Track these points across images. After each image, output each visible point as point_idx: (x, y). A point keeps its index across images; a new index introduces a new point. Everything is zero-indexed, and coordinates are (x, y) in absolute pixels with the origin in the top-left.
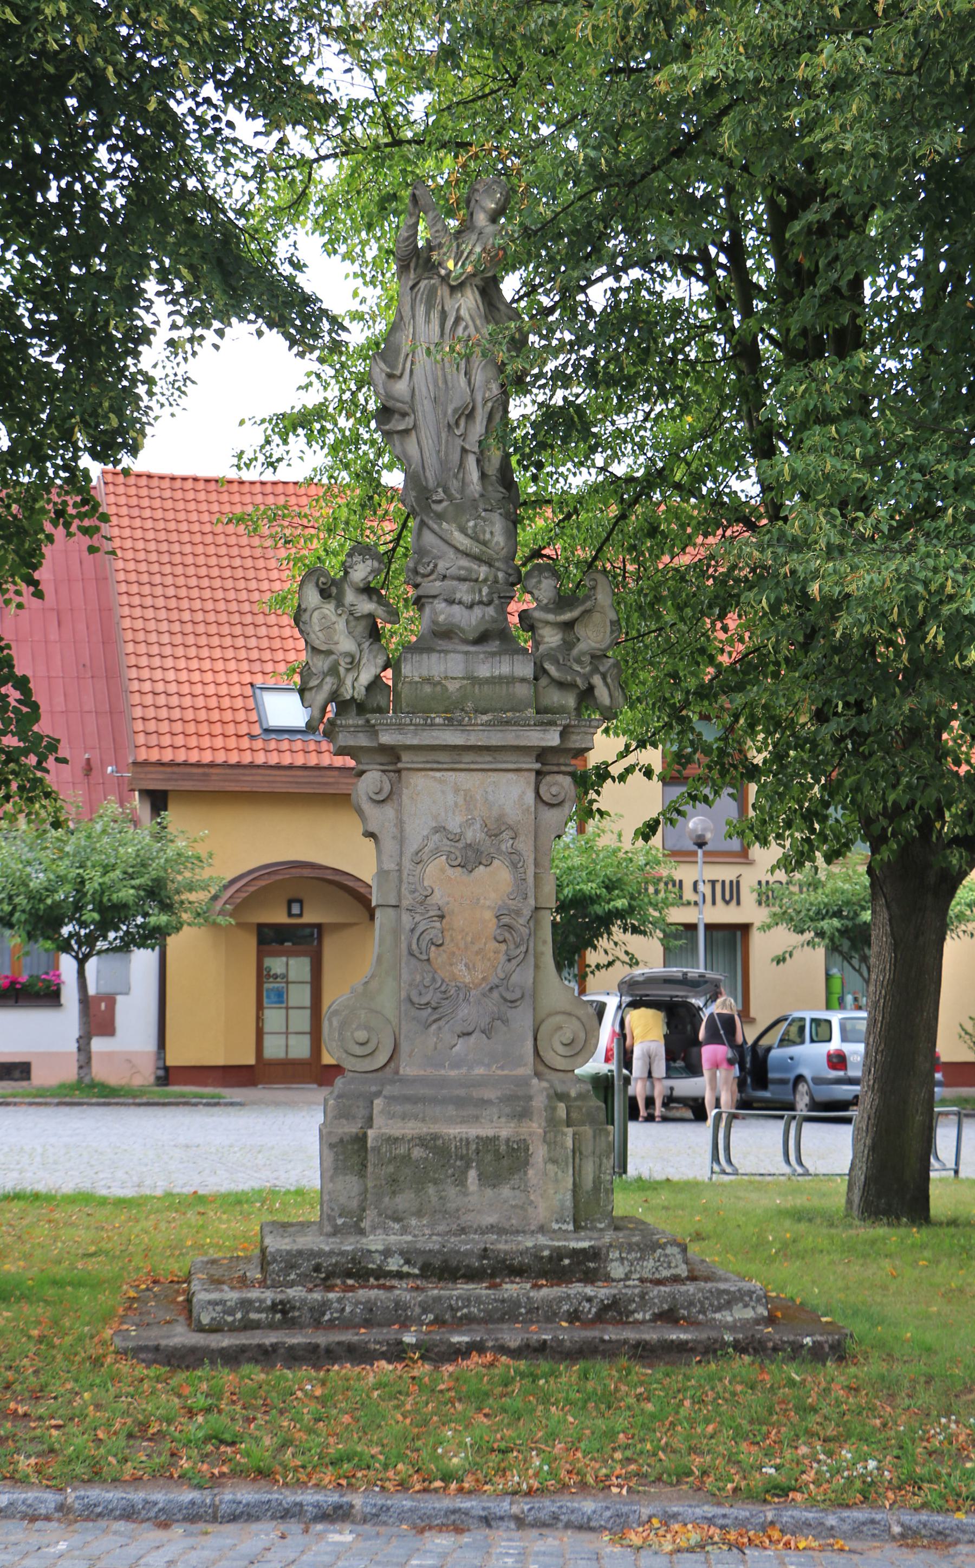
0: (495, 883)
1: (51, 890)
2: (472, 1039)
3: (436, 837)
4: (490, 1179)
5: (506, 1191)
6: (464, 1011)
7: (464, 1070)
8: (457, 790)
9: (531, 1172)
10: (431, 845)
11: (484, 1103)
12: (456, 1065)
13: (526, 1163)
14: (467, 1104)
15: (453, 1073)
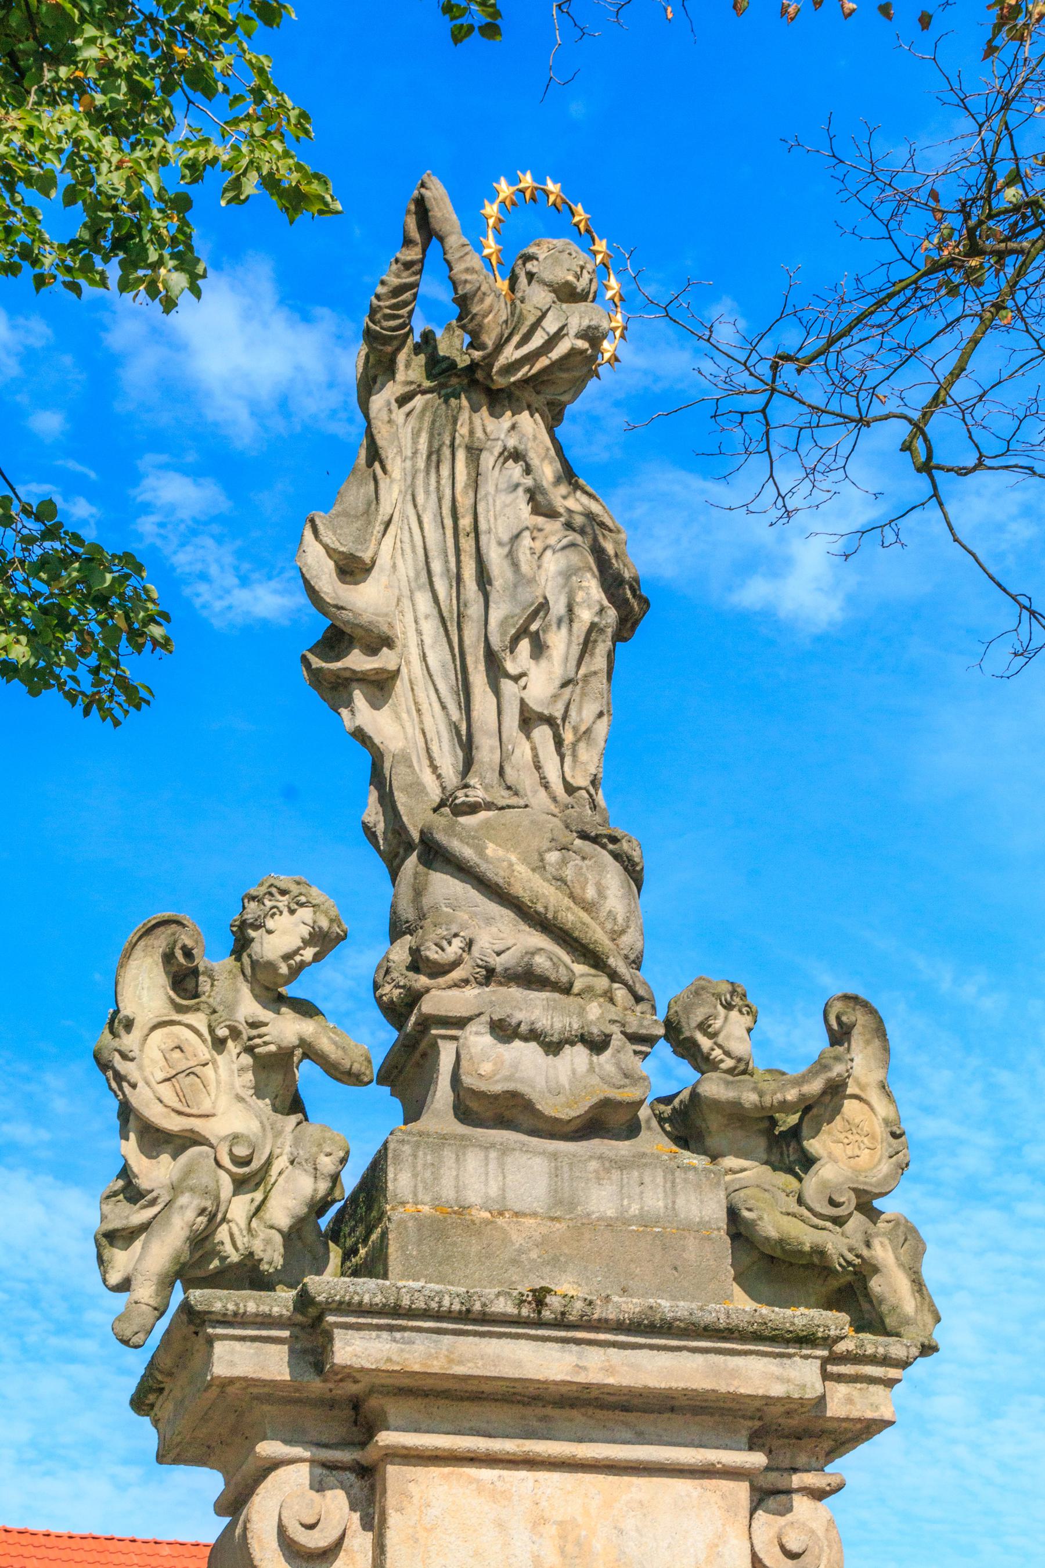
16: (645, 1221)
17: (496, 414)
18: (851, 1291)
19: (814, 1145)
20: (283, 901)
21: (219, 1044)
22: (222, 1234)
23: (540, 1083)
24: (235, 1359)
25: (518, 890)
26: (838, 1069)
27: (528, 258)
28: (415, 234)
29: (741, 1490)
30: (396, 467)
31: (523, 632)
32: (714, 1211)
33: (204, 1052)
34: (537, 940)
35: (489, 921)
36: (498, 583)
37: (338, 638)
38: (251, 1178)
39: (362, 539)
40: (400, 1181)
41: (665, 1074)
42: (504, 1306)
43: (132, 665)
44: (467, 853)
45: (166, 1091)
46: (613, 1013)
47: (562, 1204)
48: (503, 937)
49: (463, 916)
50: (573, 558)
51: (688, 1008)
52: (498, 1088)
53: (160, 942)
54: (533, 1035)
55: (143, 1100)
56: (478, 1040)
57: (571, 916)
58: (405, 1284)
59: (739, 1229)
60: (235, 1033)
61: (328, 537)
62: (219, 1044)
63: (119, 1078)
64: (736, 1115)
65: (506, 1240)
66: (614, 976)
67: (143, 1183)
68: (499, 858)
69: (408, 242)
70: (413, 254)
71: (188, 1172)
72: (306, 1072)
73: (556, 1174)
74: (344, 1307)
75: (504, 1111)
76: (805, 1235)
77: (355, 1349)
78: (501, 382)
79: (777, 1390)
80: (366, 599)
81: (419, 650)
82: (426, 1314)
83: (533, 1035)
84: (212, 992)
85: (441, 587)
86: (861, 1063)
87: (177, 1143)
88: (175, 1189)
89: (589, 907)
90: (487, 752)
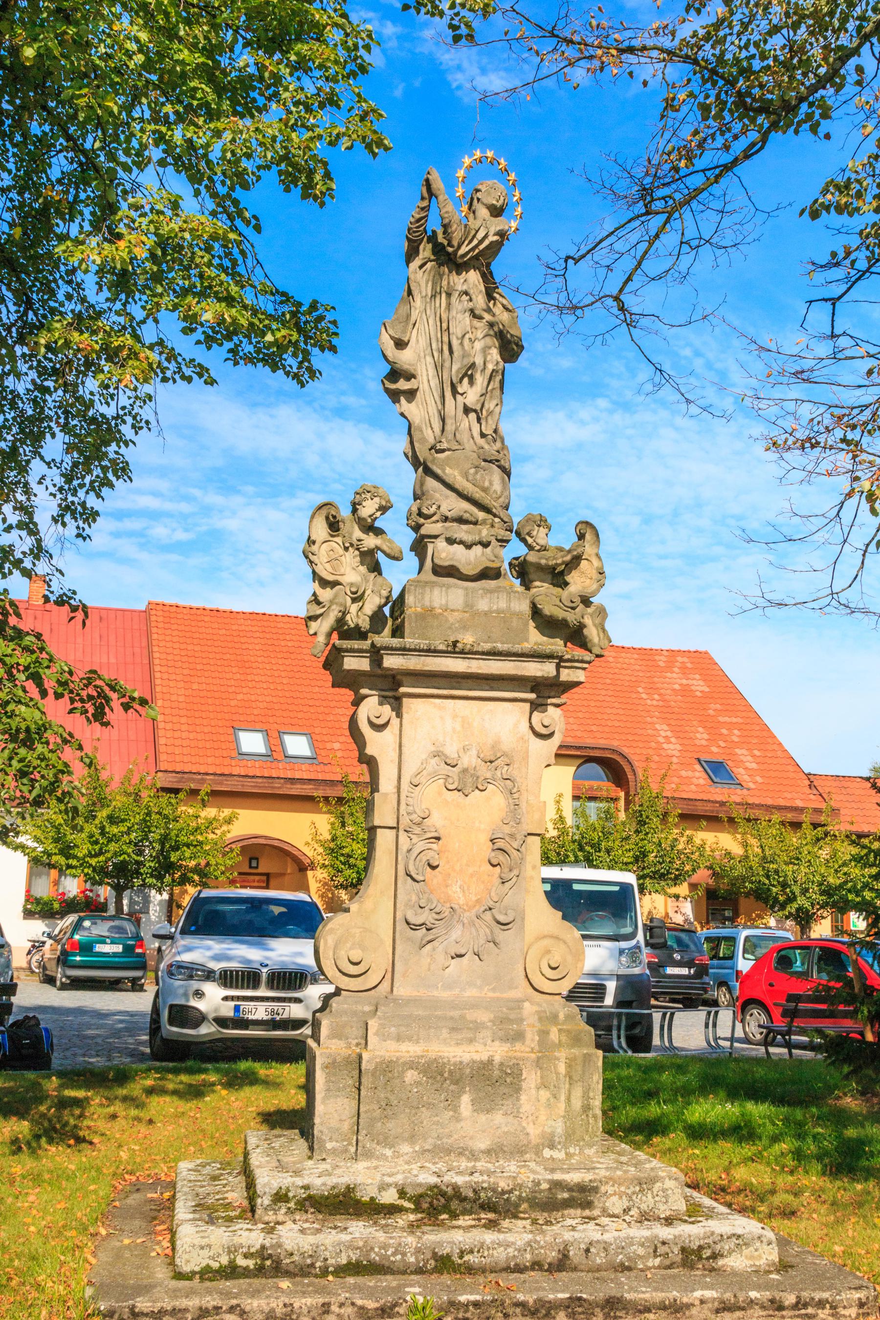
0: (486, 809)
1: (510, 1192)
2: (464, 960)
3: (434, 761)
4: (485, 1104)
5: (498, 1118)
6: (456, 933)
7: (457, 991)
8: (455, 717)
9: (523, 1097)
10: (430, 768)
11: (477, 1027)
12: (448, 987)
13: (518, 1090)
14: (462, 1028)
15: (445, 995)
16: (498, 612)
17: (459, 274)
18: (575, 635)
19: (568, 578)
20: (368, 495)
21: (346, 549)
22: (348, 617)
23: (463, 560)
24: (351, 663)
25: (457, 486)
26: (580, 550)
27: (477, 191)
28: (426, 195)
29: (527, 706)
30: (418, 298)
31: (465, 375)
32: (524, 607)
33: (341, 551)
34: (466, 505)
35: (447, 497)
36: (456, 354)
37: (395, 374)
38: (358, 598)
39: (404, 332)
40: (410, 599)
41: (516, 549)
42: (442, 647)
43: (318, 359)
44: (439, 471)
45: (328, 566)
46: (493, 531)
47: (469, 606)
48: (452, 505)
49: (437, 495)
50: (488, 340)
51: (523, 526)
52: (446, 564)
53: (324, 512)
54: (461, 542)
55: (319, 569)
56: (441, 544)
57: (478, 495)
58: (409, 641)
59: (536, 612)
60: (352, 545)
61: (391, 332)
62: (346, 549)
63: (311, 562)
64: (539, 567)
65: (447, 620)
66: (495, 516)
67: (321, 599)
68: (452, 474)
69: (423, 198)
70: (425, 204)
71: (336, 596)
72: (380, 556)
73: (467, 595)
74: (386, 648)
75: (450, 572)
76: (560, 614)
77: (391, 662)
78: (460, 261)
79: (539, 674)
80: (405, 358)
81: (426, 380)
82: (415, 650)
83: (461, 542)
84: (344, 528)
85: (436, 354)
86: (589, 549)
87: (334, 584)
88: (332, 602)
89: (485, 490)
90: (450, 427)
